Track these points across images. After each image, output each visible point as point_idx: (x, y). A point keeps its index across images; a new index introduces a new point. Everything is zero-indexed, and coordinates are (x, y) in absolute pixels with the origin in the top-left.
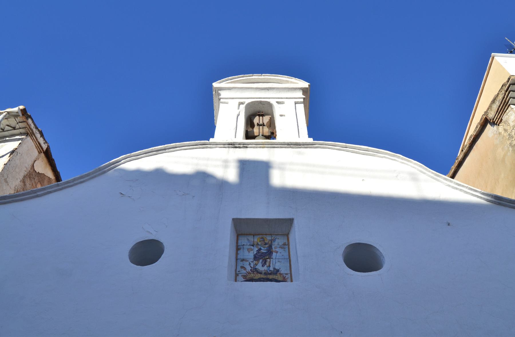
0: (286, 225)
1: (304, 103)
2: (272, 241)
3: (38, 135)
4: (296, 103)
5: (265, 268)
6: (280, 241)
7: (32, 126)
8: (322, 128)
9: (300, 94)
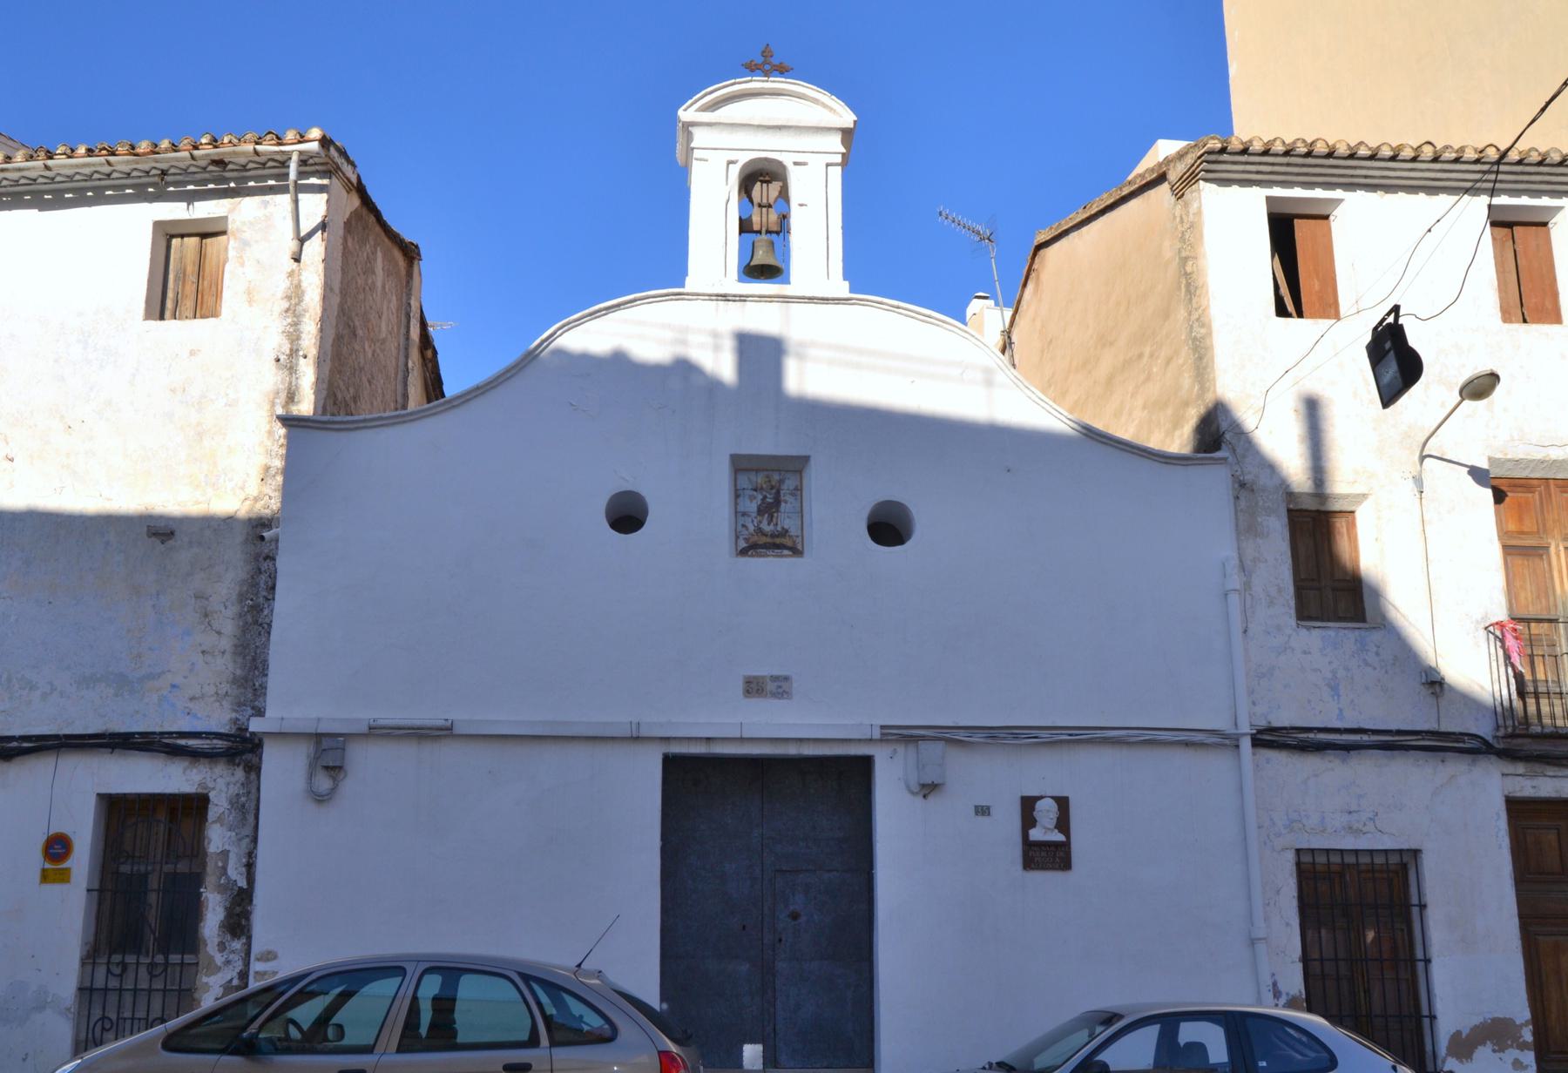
0: (797, 465)
2: (781, 482)
4: (828, 165)
5: (772, 527)
8: (875, 267)
9: (835, 144)
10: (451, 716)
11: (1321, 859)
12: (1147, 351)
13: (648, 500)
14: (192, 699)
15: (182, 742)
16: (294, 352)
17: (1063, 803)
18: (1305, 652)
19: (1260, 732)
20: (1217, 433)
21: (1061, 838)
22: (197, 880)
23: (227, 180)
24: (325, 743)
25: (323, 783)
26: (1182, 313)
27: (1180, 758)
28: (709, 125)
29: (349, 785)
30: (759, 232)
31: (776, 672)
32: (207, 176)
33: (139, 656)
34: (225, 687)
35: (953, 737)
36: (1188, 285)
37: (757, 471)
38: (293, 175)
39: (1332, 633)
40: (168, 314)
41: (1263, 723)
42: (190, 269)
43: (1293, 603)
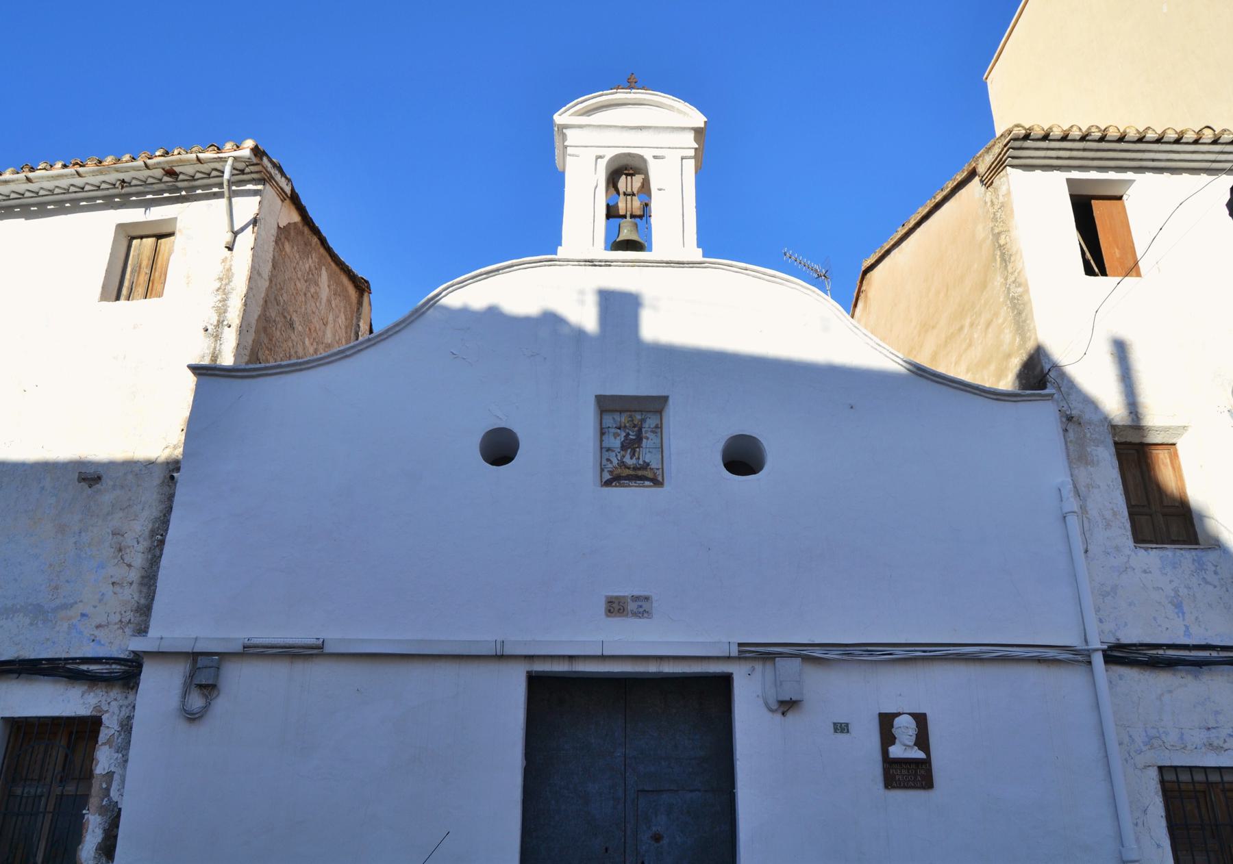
0: (656, 405)
1: (696, 157)
2: (643, 421)
3: (278, 177)
5: (634, 461)
6: (651, 422)
7: (269, 165)
8: (722, 235)
9: (689, 140)
10: (322, 636)
11: (1185, 777)
12: (967, 322)
13: (519, 435)
14: (98, 627)
15: (84, 667)
16: (220, 323)
17: (921, 720)
18: (1145, 572)
19: (1111, 648)
20: (1038, 374)
21: (921, 755)
22: (82, 801)
23: (179, 190)
24: (202, 661)
25: (196, 701)
26: (999, 280)
27: (1033, 674)
28: (580, 127)
29: (221, 704)
30: (624, 217)
31: (636, 593)
32: (162, 186)
33: (56, 588)
34: (129, 615)
35: (812, 655)
36: (1003, 255)
37: (621, 412)
38: (227, 176)
39: (1169, 553)
40: (122, 297)
41: (1112, 640)
42: (144, 263)
43: (1128, 526)
